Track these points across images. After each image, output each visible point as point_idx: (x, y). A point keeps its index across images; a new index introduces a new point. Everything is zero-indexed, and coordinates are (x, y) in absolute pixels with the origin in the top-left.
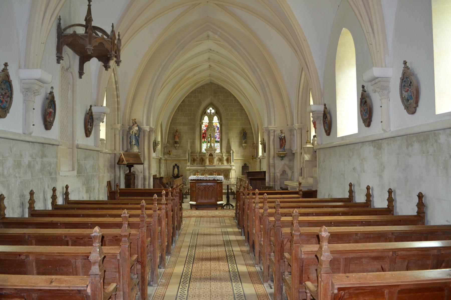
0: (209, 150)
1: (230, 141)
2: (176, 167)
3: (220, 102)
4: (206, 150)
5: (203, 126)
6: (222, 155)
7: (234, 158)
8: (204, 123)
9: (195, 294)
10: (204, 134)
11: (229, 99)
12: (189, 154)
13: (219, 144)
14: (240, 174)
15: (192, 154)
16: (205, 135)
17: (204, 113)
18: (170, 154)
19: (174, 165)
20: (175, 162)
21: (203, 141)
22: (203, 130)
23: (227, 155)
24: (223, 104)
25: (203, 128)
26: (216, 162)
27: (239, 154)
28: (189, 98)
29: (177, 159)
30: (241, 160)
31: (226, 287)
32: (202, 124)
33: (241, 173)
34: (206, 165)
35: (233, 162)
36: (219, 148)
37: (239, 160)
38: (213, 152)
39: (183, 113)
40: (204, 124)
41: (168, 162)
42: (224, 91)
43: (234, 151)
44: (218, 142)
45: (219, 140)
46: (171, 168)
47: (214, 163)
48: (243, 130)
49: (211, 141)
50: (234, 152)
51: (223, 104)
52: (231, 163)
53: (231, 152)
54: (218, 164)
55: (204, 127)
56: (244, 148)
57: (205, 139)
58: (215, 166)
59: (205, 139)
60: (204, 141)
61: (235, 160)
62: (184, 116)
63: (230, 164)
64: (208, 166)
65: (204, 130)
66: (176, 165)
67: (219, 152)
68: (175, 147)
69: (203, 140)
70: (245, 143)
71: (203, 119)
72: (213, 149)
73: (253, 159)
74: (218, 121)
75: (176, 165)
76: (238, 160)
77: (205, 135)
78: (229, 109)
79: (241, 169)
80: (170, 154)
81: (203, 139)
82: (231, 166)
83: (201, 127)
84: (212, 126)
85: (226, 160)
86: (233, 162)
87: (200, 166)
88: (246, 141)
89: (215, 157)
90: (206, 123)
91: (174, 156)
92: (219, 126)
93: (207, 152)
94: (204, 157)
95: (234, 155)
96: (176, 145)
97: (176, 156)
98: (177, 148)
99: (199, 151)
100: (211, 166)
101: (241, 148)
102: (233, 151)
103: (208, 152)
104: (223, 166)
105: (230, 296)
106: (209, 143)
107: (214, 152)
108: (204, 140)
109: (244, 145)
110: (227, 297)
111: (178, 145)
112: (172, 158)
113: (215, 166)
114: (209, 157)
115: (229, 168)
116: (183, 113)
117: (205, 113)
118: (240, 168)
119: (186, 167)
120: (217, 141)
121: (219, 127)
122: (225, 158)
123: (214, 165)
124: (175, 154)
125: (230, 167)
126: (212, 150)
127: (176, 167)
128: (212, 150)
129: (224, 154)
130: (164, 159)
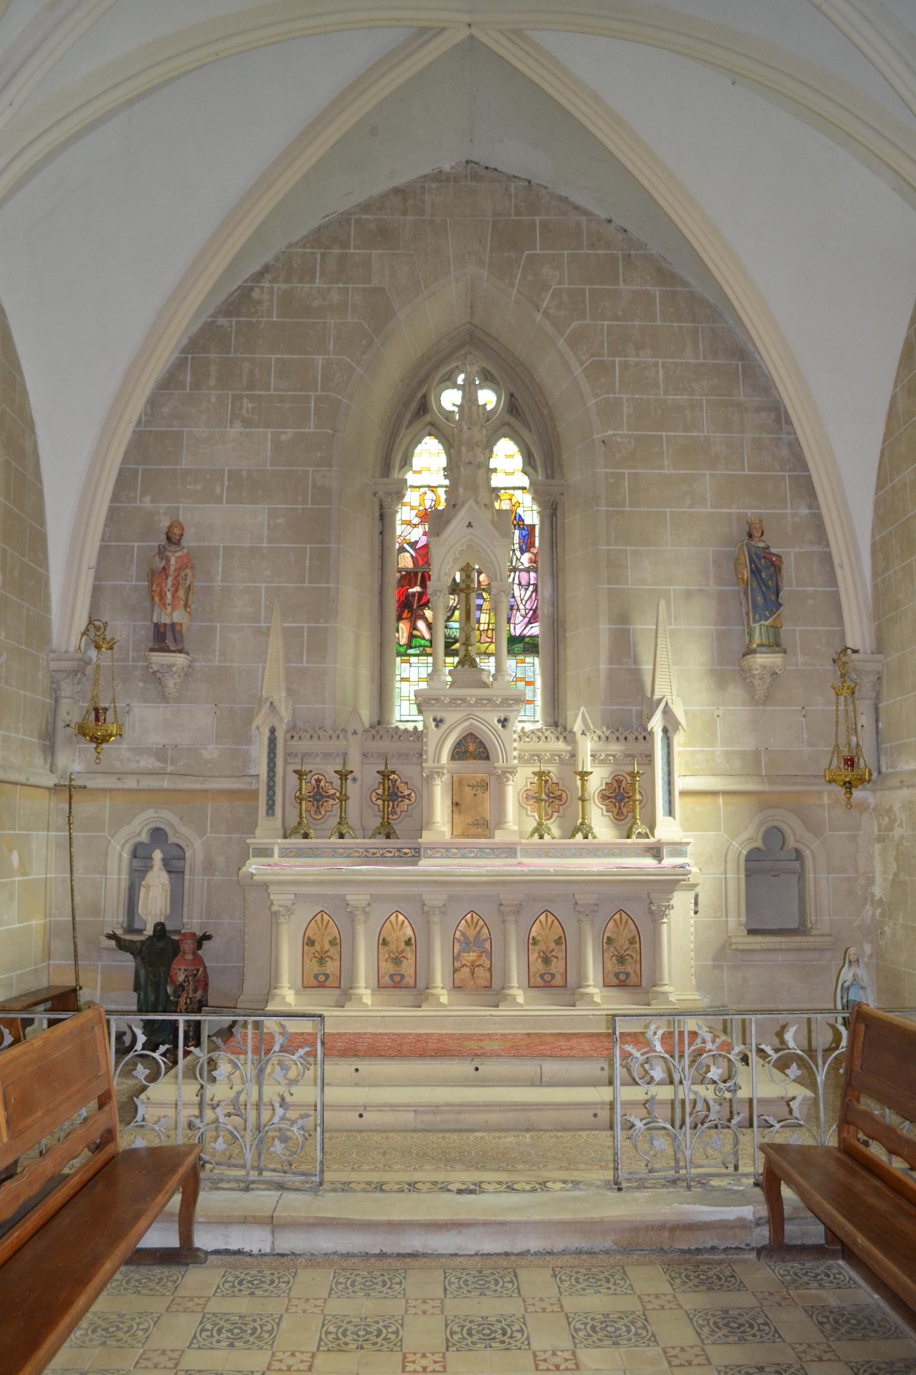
0: (454, 702)
1: (642, 627)
2: (158, 855)
3: (546, 314)
4: (423, 703)
5: (404, 514)
6: (573, 755)
7: (680, 784)
8: (411, 497)
9: (381, 1292)
10: (408, 578)
11: (622, 286)
12: (272, 741)
13: (533, 666)
14: (732, 920)
15: (304, 745)
16: (417, 589)
17: (414, 405)
18: (99, 740)
19: (144, 838)
20: (150, 813)
21: (403, 641)
22: (402, 550)
23: (615, 748)
24: (576, 324)
25: (399, 529)
26: (520, 823)
27: (719, 749)
28: (287, 280)
29: (166, 784)
30: (735, 799)
31: (496, 1276)
32: (399, 495)
33: (735, 921)
34: (427, 837)
35: (670, 812)
36: (537, 694)
37: (714, 793)
38: (493, 718)
39: (237, 399)
40: (415, 503)
41: (84, 808)
42: (578, 224)
43: (679, 711)
44: (527, 646)
45: (535, 630)
46: (113, 864)
47: (500, 821)
48: (750, 536)
49: (467, 643)
50: (676, 725)
51: (576, 324)
52: (652, 827)
53: (656, 724)
54: (539, 831)
55: (409, 523)
56: (760, 692)
57: (421, 625)
58: (509, 851)
59: (421, 625)
60: (411, 637)
61: (683, 793)
62: (247, 423)
63: (642, 829)
64: (446, 850)
65: (413, 545)
66: (158, 835)
67: (539, 725)
68: (156, 678)
69: (404, 627)
70: (775, 644)
71: (406, 462)
72: (496, 692)
73: (849, 786)
74: (525, 481)
75: (158, 835)
76: (708, 800)
77: (417, 589)
78: (625, 366)
79: (735, 879)
80: (99, 740)
81: (400, 618)
82: (656, 852)
83: (385, 519)
84: (484, 497)
85: (604, 797)
86: (670, 812)
87: (368, 856)
88: (776, 629)
89: (512, 771)
90: (430, 495)
91: (147, 762)
92: (531, 515)
93: (438, 722)
94: (404, 771)
95: (677, 749)
96: (158, 658)
97: (160, 754)
98: (171, 683)
99: (366, 715)
100: (481, 853)
101: (735, 691)
102: (667, 712)
103: (451, 717)
104: (581, 852)
105: (506, 1284)
106: (449, 652)
107: (504, 722)
108: (414, 628)
109: (761, 660)
110: (498, 1288)
111: (180, 660)
112: (120, 775)
113: (509, 851)
114: (458, 765)
115: (641, 871)
116: (237, 399)
117: (423, 408)
118: (731, 866)
119: (244, 858)
120: (521, 638)
121: (532, 527)
122: (598, 778)
123: (500, 837)
124: (155, 739)
125: (649, 862)
126: (480, 701)
127: (158, 855)
128: (480, 701)
129: (587, 746)
130: (50, 781)
